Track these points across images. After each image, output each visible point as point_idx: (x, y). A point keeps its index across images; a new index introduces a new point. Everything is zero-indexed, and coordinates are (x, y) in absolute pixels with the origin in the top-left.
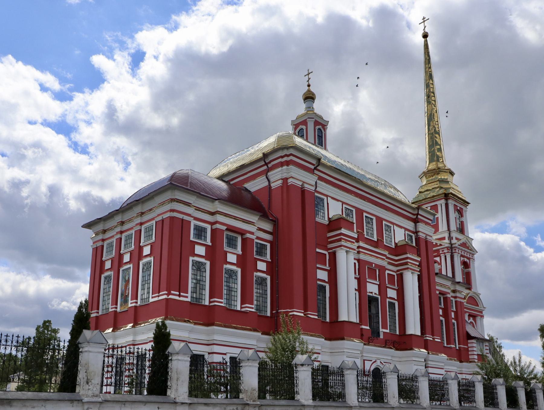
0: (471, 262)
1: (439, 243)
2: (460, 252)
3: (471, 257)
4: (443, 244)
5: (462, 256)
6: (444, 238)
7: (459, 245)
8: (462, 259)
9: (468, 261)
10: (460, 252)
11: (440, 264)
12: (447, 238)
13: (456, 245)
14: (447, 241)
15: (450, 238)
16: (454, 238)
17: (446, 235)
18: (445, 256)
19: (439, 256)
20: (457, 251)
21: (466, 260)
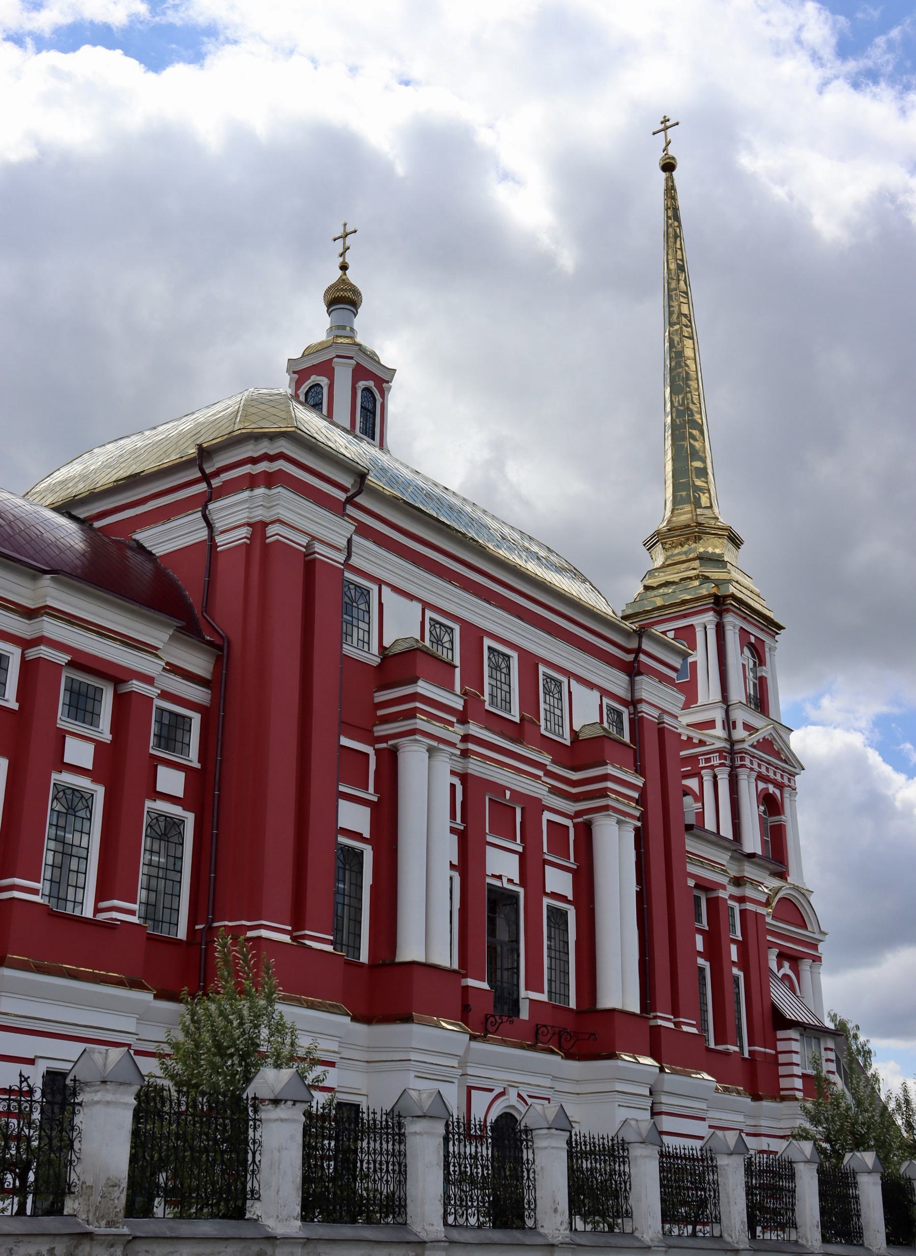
0: (786, 795)
1: (696, 735)
2: (755, 766)
3: (786, 781)
4: (708, 740)
5: (760, 777)
6: (711, 724)
7: (752, 746)
8: (761, 785)
9: (778, 792)
10: (755, 766)
11: (700, 798)
12: (719, 724)
13: (746, 746)
14: (719, 731)
15: (729, 724)
16: (740, 725)
17: (718, 715)
18: (715, 777)
19: (697, 774)
20: (747, 763)
21: (771, 789)
